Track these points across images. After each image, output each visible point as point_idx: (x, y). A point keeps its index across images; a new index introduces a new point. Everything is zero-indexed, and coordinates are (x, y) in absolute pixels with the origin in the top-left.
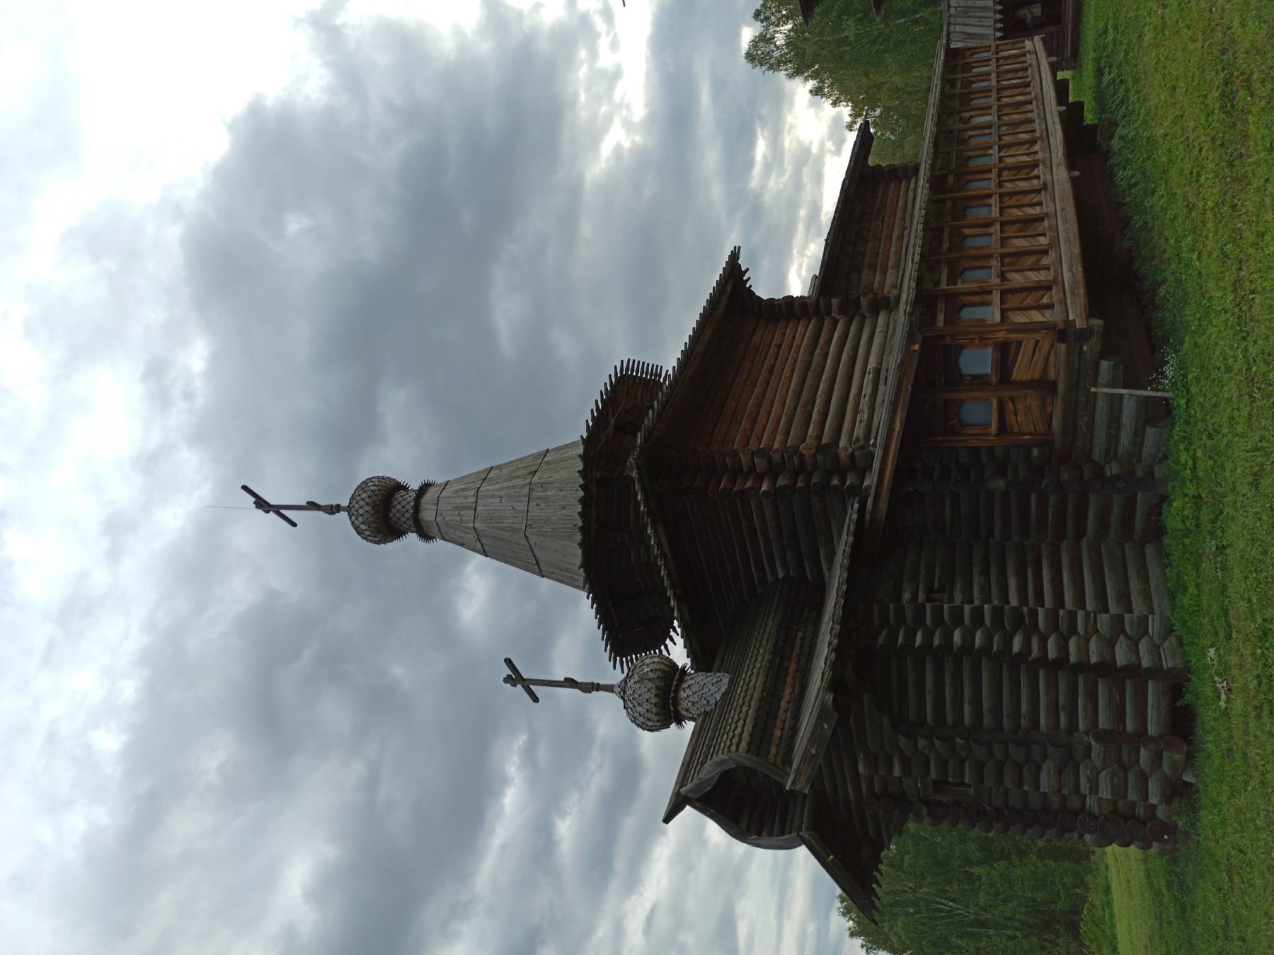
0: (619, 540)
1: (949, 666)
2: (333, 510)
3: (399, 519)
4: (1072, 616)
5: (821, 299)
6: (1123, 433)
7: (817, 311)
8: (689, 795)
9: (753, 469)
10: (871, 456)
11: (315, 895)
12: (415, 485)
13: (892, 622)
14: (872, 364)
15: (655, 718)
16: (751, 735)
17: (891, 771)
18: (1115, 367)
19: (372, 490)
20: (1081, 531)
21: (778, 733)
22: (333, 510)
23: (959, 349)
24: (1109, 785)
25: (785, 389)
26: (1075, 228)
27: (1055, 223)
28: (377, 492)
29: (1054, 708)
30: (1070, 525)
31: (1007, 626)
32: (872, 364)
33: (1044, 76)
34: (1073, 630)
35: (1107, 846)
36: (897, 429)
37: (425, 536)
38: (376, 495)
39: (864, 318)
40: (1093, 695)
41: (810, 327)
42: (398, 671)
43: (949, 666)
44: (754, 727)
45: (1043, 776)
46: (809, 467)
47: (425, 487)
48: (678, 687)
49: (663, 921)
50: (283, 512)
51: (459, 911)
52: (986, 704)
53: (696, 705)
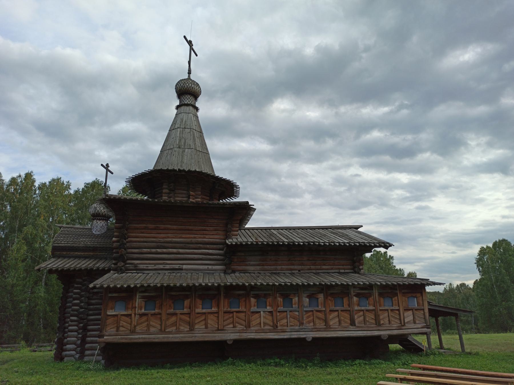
0: (37, 210)
2: (189, 73)
3: (186, 98)
11: (318, 49)
12: (197, 105)
14: (184, 267)
15: (92, 213)
16: (59, 246)
19: (185, 86)
21: (64, 253)
22: (189, 73)
25: (174, 237)
27: (196, 333)
28: (185, 88)
32: (184, 267)
33: (369, 332)
35: (464, 347)
37: (178, 107)
38: (184, 89)
42: (415, 39)
44: (63, 246)
47: (197, 109)
48: (98, 219)
49: (357, 179)
50: (192, 52)
51: (331, 103)
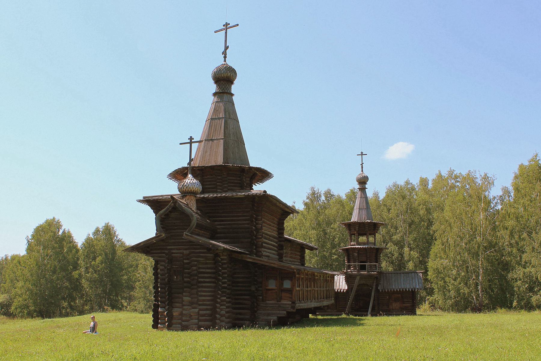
1: (213, 276)
4: (224, 305)
5: (284, 239)
6: (266, 317)
7: (280, 237)
8: (177, 203)
9: (257, 224)
10: (260, 257)
13: (222, 261)
17: (186, 259)
18: (284, 314)
20: (235, 309)
23: (292, 280)
24: (186, 313)
26: (306, 308)
29: (204, 300)
30: (237, 306)
31: (223, 290)
34: (222, 305)
36: (272, 265)
39: (277, 251)
40: (207, 310)
41: (276, 235)
43: (213, 276)
45: (187, 298)
46: (257, 240)
52: (204, 284)
53: (190, 202)
